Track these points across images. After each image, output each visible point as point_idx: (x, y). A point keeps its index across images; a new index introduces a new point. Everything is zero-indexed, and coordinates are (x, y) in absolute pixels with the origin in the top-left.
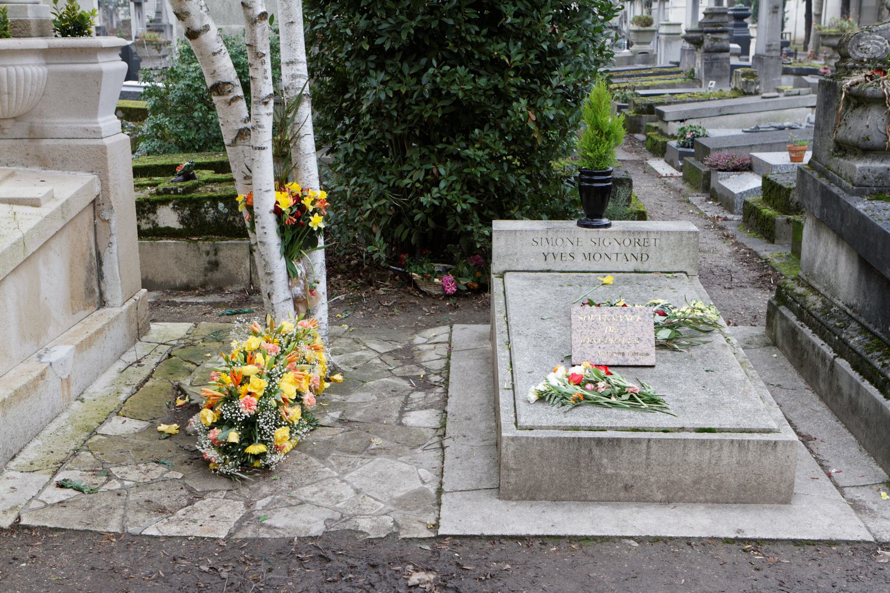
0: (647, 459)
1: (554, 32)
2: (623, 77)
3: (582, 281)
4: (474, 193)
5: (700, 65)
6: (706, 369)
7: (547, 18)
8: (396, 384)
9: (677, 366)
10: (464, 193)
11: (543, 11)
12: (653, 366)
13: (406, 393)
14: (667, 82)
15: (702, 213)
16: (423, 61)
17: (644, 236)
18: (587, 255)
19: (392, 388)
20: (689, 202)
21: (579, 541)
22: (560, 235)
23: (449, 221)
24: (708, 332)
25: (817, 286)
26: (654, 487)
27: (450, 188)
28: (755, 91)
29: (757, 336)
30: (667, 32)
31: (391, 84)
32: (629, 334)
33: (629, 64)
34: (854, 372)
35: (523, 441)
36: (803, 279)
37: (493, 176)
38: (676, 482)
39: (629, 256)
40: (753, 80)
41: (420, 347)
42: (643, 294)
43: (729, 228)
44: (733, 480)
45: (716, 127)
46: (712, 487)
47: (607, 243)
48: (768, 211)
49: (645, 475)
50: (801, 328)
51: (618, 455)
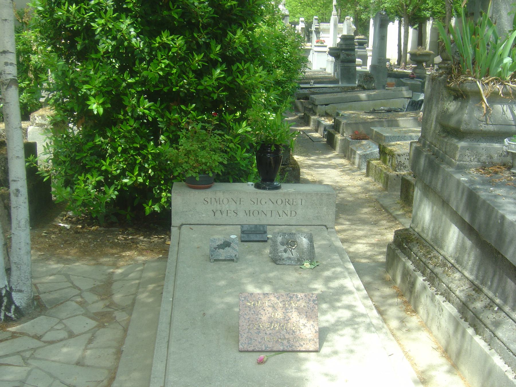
39: (281, 212)
47: (263, 202)
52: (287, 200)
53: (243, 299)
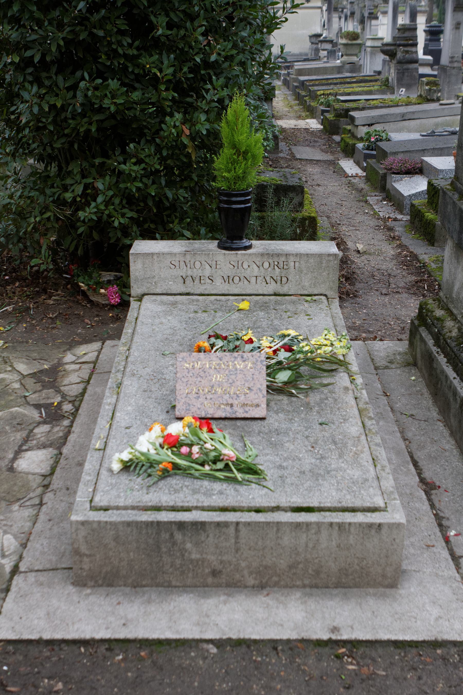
0: (236, 543)
1: (209, 44)
2: (331, 84)
3: (219, 307)
4: (134, 207)
5: (393, 75)
6: (320, 421)
7: (199, 29)
8: (25, 415)
9: (290, 417)
10: (124, 207)
11: (196, 23)
12: (263, 419)
13: (31, 427)
14: (366, 89)
15: (375, 213)
16: (78, 74)
17: (283, 259)
18: (226, 278)
19: (18, 420)
20: (366, 201)
21: (151, 645)
22: (198, 258)
23: (111, 235)
24: (332, 370)
25: (455, 311)
26: (246, 572)
27: (107, 203)
28: (437, 98)
29: (400, 354)
30: (372, 45)
31: (47, 97)
32: (238, 383)
33: (339, 73)
35: (95, 526)
36: (443, 301)
37: (149, 191)
38: (269, 567)
39: (268, 279)
40: (435, 88)
41: (67, 367)
42: (276, 322)
43: (397, 229)
44: (333, 565)
45: (399, 131)
46: (310, 571)
47: (245, 266)
48: (430, 215)
49: (234, 560)
50: (437, 355)
51: (203, 539)
53: (181, 360)
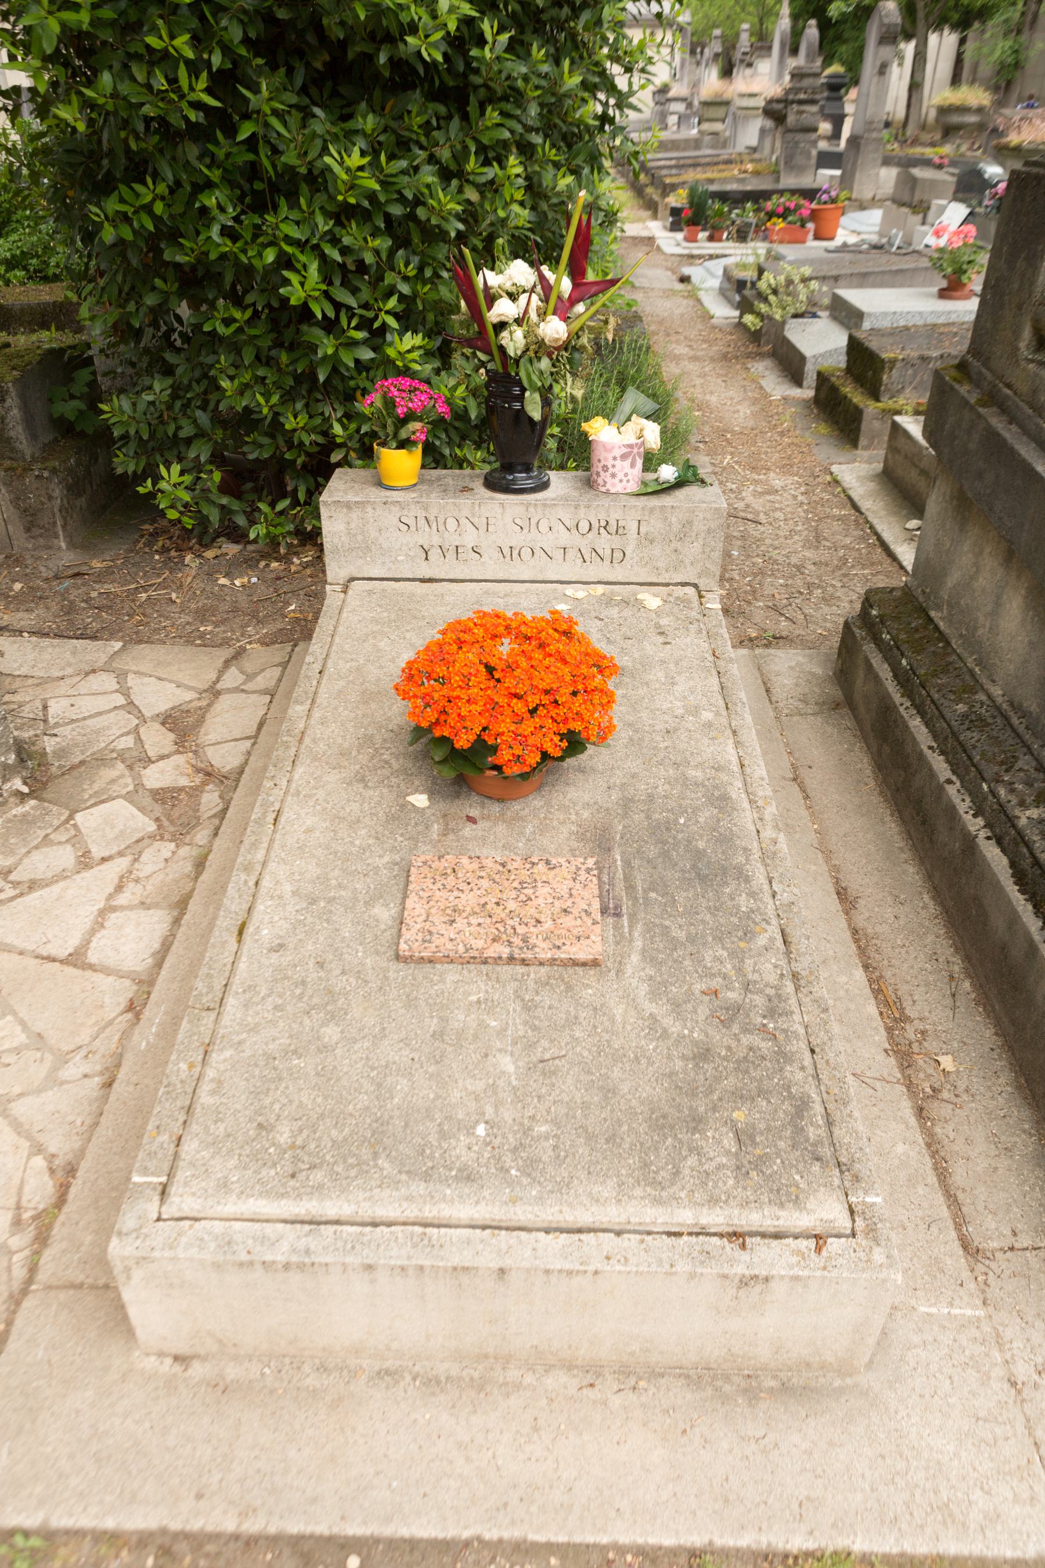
18: (506, 551)
34: (1021, 897)
52: (603, 523)
